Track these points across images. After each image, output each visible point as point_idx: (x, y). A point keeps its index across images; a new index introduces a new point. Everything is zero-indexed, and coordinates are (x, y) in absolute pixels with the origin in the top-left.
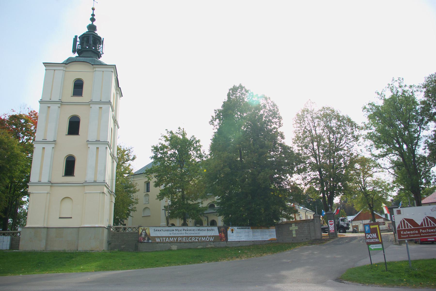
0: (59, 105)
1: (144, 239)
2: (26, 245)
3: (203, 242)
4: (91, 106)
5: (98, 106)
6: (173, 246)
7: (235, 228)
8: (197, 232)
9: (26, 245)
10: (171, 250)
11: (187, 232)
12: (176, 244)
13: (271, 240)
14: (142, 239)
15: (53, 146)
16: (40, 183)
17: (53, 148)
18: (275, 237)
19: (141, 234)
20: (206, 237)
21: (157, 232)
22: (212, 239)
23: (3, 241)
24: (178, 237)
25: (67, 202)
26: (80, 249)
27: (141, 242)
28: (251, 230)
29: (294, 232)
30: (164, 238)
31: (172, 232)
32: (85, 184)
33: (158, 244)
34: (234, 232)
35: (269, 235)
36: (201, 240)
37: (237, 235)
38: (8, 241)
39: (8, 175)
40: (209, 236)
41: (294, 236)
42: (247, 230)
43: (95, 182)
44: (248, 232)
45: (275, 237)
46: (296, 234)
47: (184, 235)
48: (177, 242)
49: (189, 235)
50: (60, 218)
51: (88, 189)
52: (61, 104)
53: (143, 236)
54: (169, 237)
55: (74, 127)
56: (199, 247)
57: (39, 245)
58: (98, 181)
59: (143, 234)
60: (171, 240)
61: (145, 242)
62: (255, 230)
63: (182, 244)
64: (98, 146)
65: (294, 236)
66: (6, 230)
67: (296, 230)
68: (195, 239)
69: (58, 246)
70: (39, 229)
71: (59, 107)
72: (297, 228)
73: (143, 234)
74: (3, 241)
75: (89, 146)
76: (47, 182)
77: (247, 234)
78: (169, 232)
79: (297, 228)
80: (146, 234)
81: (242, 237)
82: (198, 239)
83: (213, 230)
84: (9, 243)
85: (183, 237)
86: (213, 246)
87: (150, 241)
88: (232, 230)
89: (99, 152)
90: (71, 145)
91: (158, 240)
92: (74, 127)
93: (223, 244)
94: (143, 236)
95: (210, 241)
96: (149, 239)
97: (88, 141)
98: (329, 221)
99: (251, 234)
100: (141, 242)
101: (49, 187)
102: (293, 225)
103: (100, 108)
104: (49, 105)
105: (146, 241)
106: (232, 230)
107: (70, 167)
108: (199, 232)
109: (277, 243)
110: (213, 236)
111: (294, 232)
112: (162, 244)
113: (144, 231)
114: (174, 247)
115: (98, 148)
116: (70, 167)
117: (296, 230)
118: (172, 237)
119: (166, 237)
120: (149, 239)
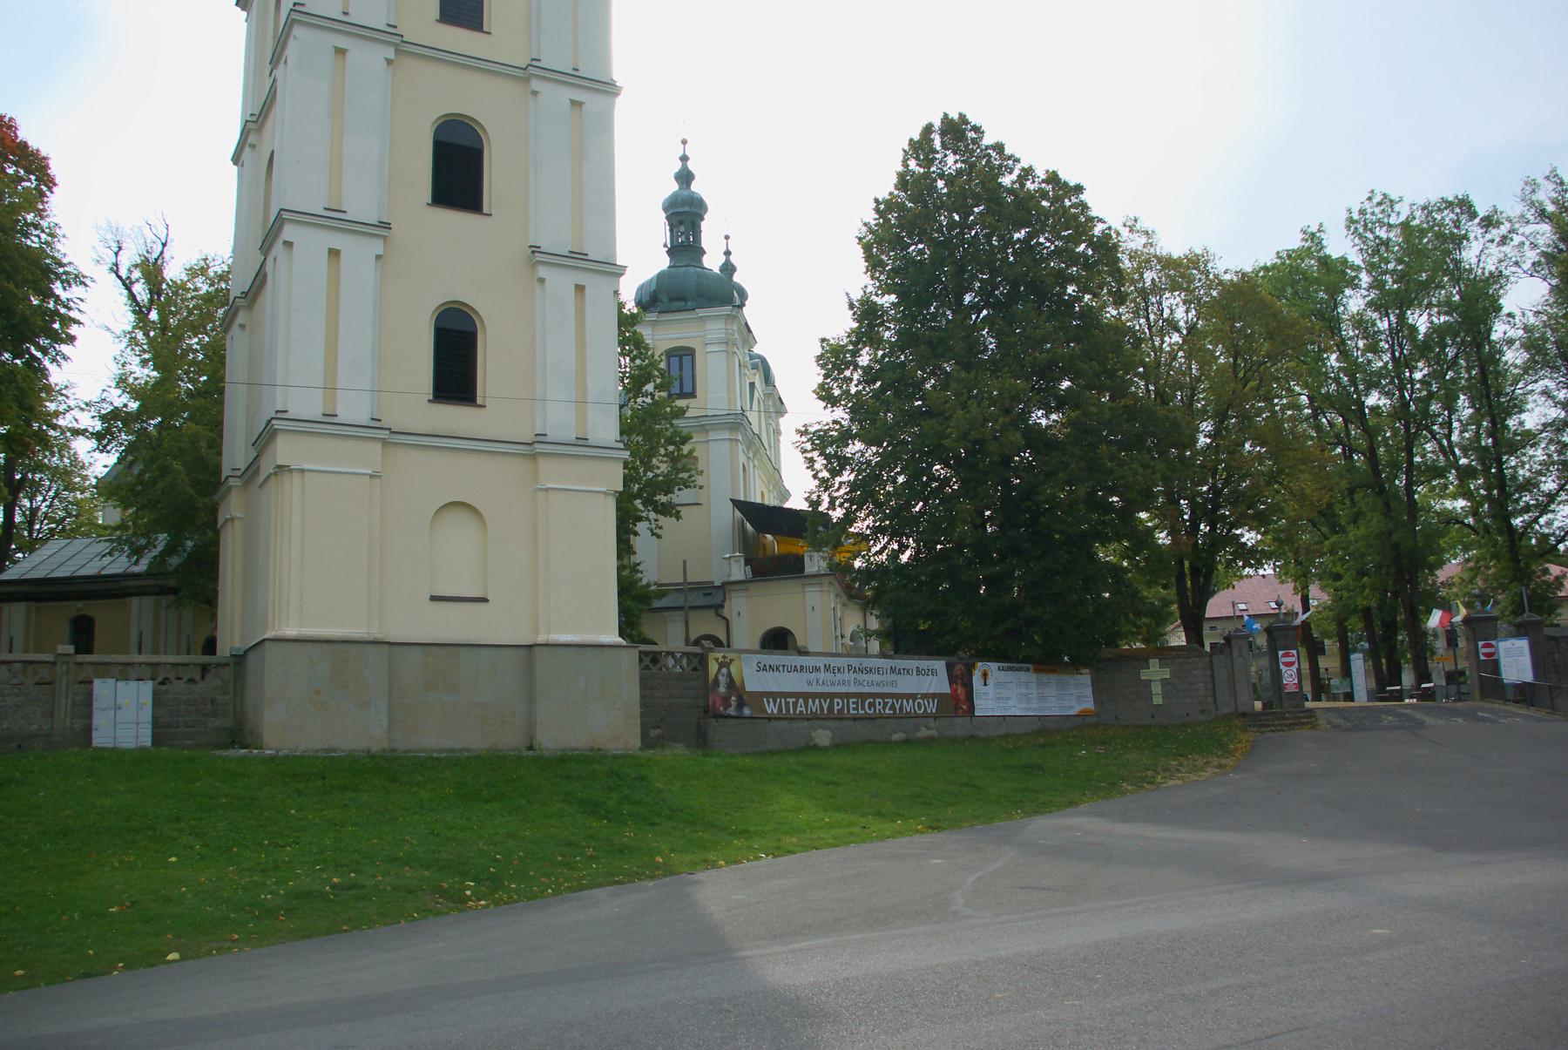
0: (391, 53)
1: (726, 701)
2: (289, 721)
3: (908, 716)
4: (535, 85)
5: (567, 94)
6: (820, 731)
7: (993, 666)
8: (889, 677)
9: (289, 721)
10: (815, 747)
11: (861, 677)
12: (828, 724)
13: (1083, 715)
14: (718, 702)
15: (378, 247)
16: (328, 425)
17: (378, 257)
18: (1089, 705)
19: (716, 681)
20: (913, 696)
21: (769, 675)
22: (932, 708)
23: (117, 708)
24: (832, 696)
25: (461, 526)
26: (550, 739)
27: (718, 716)
28: (1031, 677)
29: (1156, 689)
30: (791, 700)
31: (813, 676)
32: (534, 449)
33: (773, 723)
34: (990, 680)
35: (1071, 696)
36: (901, 708)
37: (1003, 693)
38: (140, 707)
39: (1114, 313)
40: (925, 696)
41: (1158, 700)
42: (1022, 675)
43: (582, 441)
44: (1027, 684)
45: (1089, 705)
46: (1165, 695)
47: (853, 689)
48: (831, 717)
49: (866, 690)
50: (434, 598)
51: (552, 473)
52: (397, 51)
53: (722, 689)
54: (806, 696)
55: (458, 172)
56: (895, 737)
57: (360, 729)
58: (590, 442)
59: (723, 680)
60: (814, 706)
61: (730, 716)
62: (1045, 677)
63: (845, 723)
64: (582, 278)
65: (1158, 700)
66: (89, 651)
67: (1164, 683)
68: (885, 704)
69: (441, 731)
70: (352, 647)
71: (389, 62)
72: (1166, 674)
73: (723, 680)
74: (117, 708)
75: (542, 272)
76: (365, 421)
77: (1023, 691)
78: (805, 676)
79: (1166, 674)
80: (731, 684)
81: (1011, 703)
82: (893, 707)
83: (934, 672)
84: (147, 715)
85: (848, 695)
86: (934, 733)
87: (747, 712)
88: (985, 675)
89: (589, 310)
90: (459, 258)
91: (771, 708)
92: (458, 172)
93: (961, 725)
94: (722, 689)
95: (926, 716)
96: (741, 704)
97: (535, 249)
98: (1480, 644)
99: (1034, 691)
100: (718, 716)
101: (378, 447)
102: (1154, 662)
103: (573, 102)
104: (342, 42)
105: (732, 711)
106: (985, 675)
107: (455, 363)
108: (894, 677)
109: (1096, 726)
110: (934, 696)
111: (1156, 689)
112: (784, 724)
113: (724, 670)
114: (823, 737)
115: (580, 289)
116: (455, 363)
117: (1164, 683)
118: (814, 696)
119: (797, 695)
120: (741, 704)
